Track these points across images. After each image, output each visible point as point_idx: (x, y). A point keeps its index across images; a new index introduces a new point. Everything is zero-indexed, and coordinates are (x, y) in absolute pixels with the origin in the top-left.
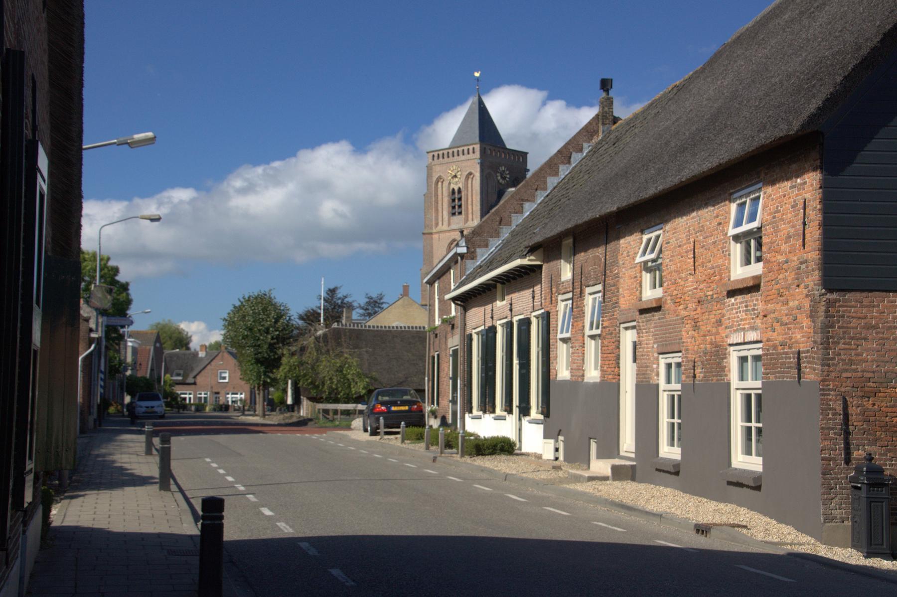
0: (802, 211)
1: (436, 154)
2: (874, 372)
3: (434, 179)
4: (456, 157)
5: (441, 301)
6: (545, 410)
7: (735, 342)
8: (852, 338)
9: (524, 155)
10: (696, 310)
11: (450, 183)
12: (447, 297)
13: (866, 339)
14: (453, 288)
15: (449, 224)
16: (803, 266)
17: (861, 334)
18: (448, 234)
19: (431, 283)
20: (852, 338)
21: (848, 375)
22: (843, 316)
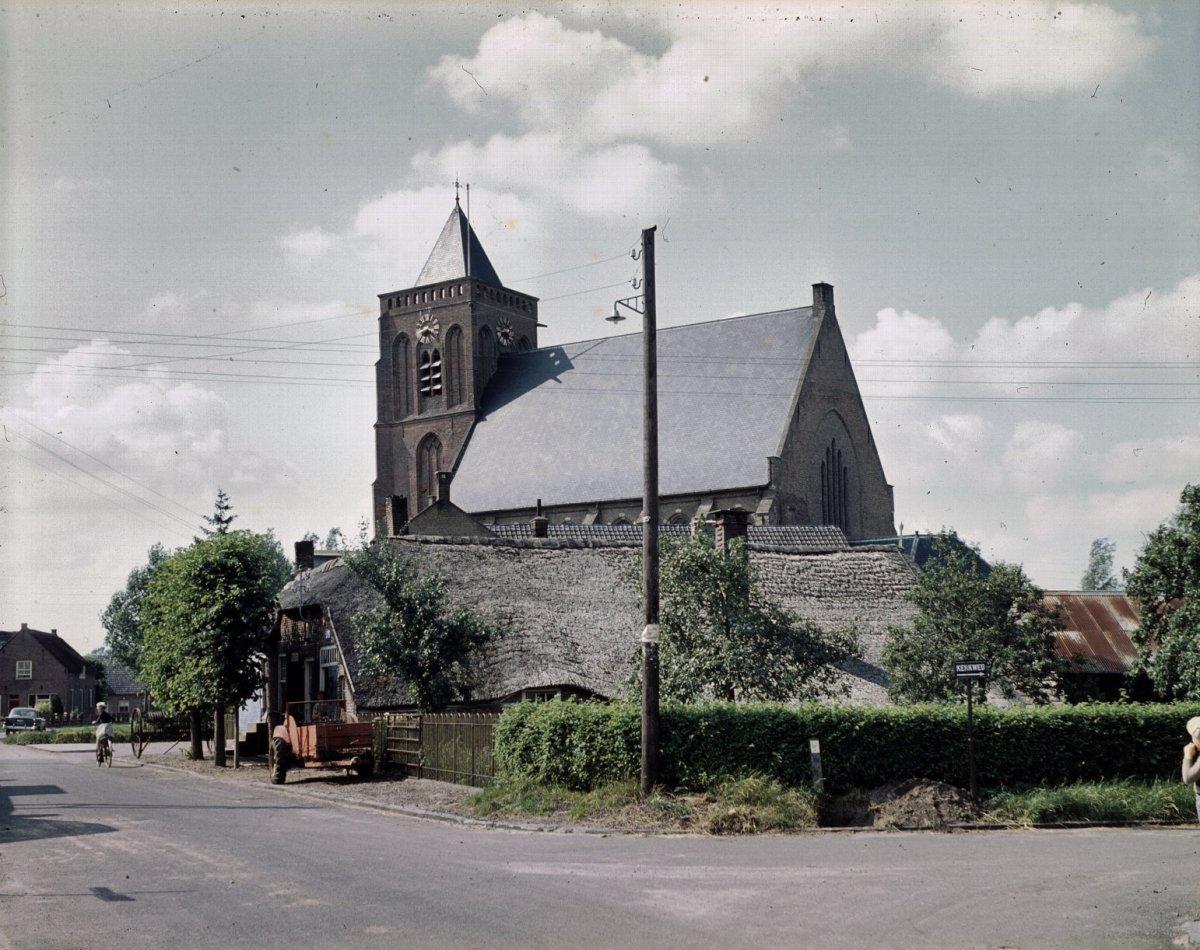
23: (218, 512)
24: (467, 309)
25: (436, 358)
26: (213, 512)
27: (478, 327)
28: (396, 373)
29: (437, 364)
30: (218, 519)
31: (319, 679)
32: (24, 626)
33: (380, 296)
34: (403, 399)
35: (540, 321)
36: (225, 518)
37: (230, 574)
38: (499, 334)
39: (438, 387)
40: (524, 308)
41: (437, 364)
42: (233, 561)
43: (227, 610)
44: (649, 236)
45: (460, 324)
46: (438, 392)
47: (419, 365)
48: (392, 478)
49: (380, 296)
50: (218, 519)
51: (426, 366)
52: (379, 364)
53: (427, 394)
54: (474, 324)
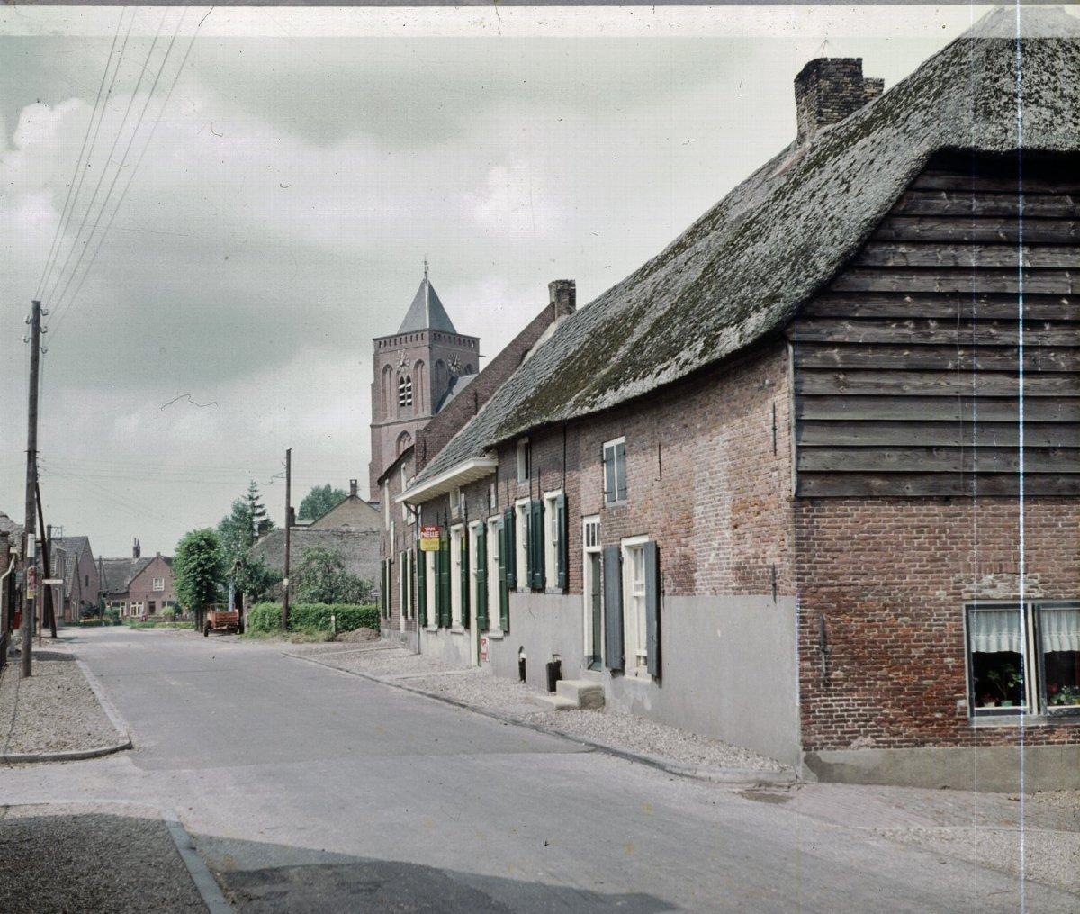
0: (772, 415)
1: (403, 337)
2: (850, 585)
3: (382, 367)
4: (388, 347)
5: (391, 503)
6: (564, 584)
7: (615, 760)
8: (827, 551)
9: (475, 341)
10: (743, 426)
11: (398, 372)
12: (398, 500)
13: (841, 551)
14: (404, 489)
15: (398, 416)
16: (775, 474)
17: (836, 545)
18: (399, 426)
19: (381, 482)
20: (827, 551)
21: (825, 589)
22: (818, 527)
23: (250, 494)
24: (427, 350)
25: (409, 381)
26: (247, 493)
27: (434, 362)
28: (384, 391)
29: (409, 385)
30: (251, 498)
31: (528, 548)
32: (158, 553)
33: (374, 340)
34: (389, 408)
35: (480, 354)
36: (255, 497)
37: (200, 548)
38: (450, 364)
39: (409, 401)
40: (470, 345)
41: (409, 385)
42: (203, 543)
43: (200, 565)
44: (289, 452)
45: (422, 359)
46: (410, 404)
47: (397, 386)
48: (381, 460)
49: (374, 340)
50: (251, 498)
51: (402, 387)
52: (373, 385)
53: (403, 405)
54: (431, 359)
